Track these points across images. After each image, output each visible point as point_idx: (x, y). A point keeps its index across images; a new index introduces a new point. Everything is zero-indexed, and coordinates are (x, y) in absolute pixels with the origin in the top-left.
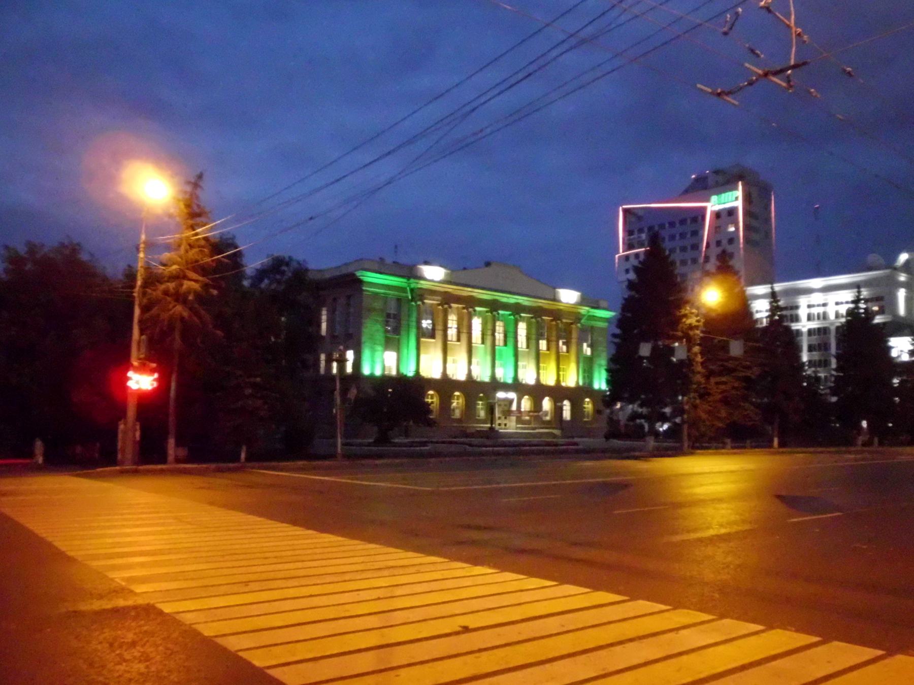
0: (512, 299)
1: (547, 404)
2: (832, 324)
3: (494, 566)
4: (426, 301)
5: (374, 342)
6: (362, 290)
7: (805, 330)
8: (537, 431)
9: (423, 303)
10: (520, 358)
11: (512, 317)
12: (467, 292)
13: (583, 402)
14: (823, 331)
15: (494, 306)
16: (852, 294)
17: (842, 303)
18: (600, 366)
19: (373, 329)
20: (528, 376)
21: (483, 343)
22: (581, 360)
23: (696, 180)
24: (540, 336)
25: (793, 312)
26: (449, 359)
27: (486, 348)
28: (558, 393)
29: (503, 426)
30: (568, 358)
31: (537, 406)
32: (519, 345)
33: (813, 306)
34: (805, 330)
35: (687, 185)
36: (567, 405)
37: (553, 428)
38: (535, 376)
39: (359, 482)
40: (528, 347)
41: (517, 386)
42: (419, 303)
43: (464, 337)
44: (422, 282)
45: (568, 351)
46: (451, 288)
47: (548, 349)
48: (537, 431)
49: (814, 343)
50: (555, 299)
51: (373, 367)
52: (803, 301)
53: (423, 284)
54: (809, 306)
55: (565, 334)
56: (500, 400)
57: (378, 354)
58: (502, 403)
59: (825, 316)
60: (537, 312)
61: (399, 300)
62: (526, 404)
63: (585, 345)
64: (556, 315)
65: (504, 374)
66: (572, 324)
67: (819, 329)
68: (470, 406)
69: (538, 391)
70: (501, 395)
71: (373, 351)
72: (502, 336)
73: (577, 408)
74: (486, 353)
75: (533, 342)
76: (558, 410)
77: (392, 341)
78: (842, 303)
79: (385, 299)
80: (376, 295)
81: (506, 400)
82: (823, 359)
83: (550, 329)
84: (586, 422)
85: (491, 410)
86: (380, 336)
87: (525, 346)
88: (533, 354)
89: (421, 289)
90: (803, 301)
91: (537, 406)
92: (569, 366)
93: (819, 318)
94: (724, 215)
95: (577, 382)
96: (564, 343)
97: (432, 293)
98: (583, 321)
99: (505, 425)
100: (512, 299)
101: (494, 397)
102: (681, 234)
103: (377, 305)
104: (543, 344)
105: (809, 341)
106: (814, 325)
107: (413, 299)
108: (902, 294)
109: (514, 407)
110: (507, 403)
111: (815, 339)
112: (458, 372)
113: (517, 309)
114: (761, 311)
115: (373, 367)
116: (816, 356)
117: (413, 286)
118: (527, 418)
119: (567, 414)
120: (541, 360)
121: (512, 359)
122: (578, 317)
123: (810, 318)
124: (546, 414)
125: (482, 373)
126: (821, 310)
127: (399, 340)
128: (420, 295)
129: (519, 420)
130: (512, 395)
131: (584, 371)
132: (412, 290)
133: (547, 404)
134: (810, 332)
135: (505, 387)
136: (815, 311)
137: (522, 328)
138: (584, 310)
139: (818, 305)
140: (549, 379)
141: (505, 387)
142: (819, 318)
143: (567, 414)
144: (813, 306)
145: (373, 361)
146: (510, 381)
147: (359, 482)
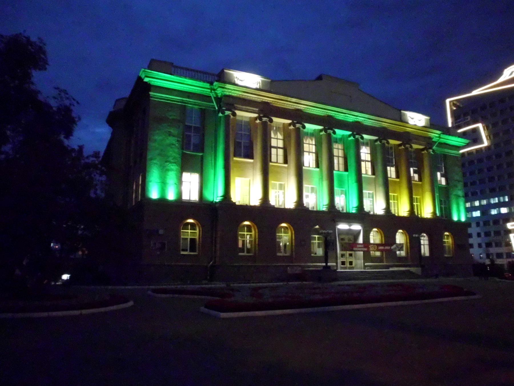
0: (351, 117)
1: (400, 238)
3: (363, 125)
4: (238, 113)
5: (165, 159)
6: (150, 100)
8: (391, 269)
9: (234, 114)
10: (364, 185)
12: (291, 103)
13: (442, 236)
15: (329, 123)
18: (458, 196)
19: (164, 140)
20: (376, 205)
21: (318, 166)
22: (436, 190)
24: (387, 163)
26: (272, 182)
27: (321, 171)
28: (413, 224)
29: (348, 265)
30: (422, 186)
31: (389, 239)
32: (363, 171)
36: (424, 241)
37: (410, 266)
38: (384, 205)
39: (45, 314)
40: (373, 173)
41: (362, 216)
42: (227, 113)
43: (292, 158)
44: (228, 86)
45: (420, 179)
46: (269, 98)
47: (398, 176)
48: (391, 269)
50: (401, 119)
51: (163, 190)
53: (230, 90)
55: (416, 160)
56: (341, 232)
57: (172, 177)
58: (346, 237)
60: (383, 134)
61: (203, 113)
62: (375, 237)
63: (439, 174)
64: (407, 137)
65: (346, 202)
66: (423, 150)
68: (302, 242)
69: (389, 223)
70: (342, 226)
71: (164, 171)
72: (341, 160)
73: (435, 244)
74: (321, 179)
75: (379, 168)
76: (414, 244)
77: (192, 159)
79: (183, 109)
80: (169, 106)
81: (349, 232)
83: (398, 155)
84: (447, 258)
85: (329, 245)
86: (174, 153)
87: (370, 172)
88: (380, 180)
89: (229, 96)
91: (389, 239)
92: (423, 197)
95: (434, 213)
96: (415, 172)
97: (246, 103)
98: (434, 147)
99: (351, 263)
100: (351, 117)
101: (334, 229)
103: (172, 115)
104: (392, 171)
107: (220, 110)
109: (361, 240)
110: (351, 237)
112: (284, 196)
113: (357, 128)
115: (163, 190)
117: (220, 92)
118: (378, 254)
119: (425, 250)
122: (429, 142)
124: (400, 247)
125: (316, 200)
127: (202, 158)
128: (231, 103)
129: (367, 257)
130: (357, 227)
131: (441, 202)
132: (219, 100)
133: (400, 238)
135: (348, 217)
137: (365, 153)
138: (435, 134)
140: (402, 209)
141: (348, 217)
143: (425, 250)
145: (164, 183)
147: (45, 314)
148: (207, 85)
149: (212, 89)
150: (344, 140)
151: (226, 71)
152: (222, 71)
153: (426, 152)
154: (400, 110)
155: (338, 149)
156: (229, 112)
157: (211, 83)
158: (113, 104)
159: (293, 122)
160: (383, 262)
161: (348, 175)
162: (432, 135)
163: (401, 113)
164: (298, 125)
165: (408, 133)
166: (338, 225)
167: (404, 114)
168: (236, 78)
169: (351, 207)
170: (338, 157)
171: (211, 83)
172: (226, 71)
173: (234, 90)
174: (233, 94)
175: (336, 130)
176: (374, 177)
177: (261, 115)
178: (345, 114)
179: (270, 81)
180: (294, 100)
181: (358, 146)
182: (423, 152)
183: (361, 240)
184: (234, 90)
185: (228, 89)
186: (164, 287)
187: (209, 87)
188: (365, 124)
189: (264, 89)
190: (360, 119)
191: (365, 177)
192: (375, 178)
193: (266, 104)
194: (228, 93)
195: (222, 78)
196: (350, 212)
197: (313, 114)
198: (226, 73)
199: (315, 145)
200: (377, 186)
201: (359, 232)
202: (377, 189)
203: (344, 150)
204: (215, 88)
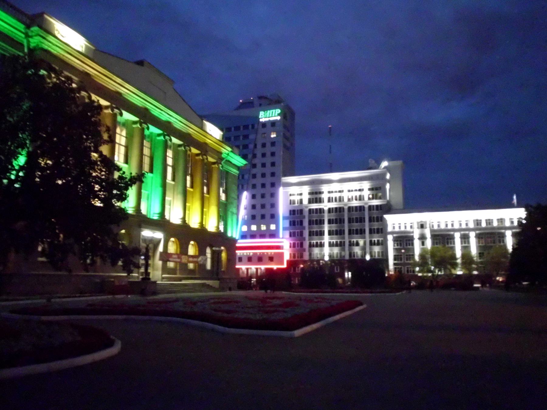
1: (192, 250)
2: (346, 205)
3: (191, 137)
7: (326, 209)
8: (184, 282)
11: (162, 138)
14: (339, 210)
16: (369, 184)
17: (352, 191)
20: (174, 216)
23: (242, 103)
25: (318, 196)
28: (203, 237)
31: (184, 250)
33: (332, 192)
34: (326, 209)
35: (239, 104)
41: (162, 224)
44: (50, 38)
48: (184, 282)
49: (331, 218)
50: (202, 127)
52: (325, 188)
54: (329, 192)
59: (341, 199)
64: (204, 148)
66: (214, 163)
67: (336, 208)
69: (183, 233)
70: (147, 233)
75: (180, 174)
78: (352, 191)
82: (338, 229)
88: (180, 188)
90: (325, 188)
91: (184, 250)
93: (336, 201)
94: (269, 126)
102: (235, 137)
105: (329, 216)
106: (333, 205)
108: (388, 186)
109: (161, 248)
111: (333, 216)
113: (168, 129)
114: (293, 195)
116: (334, 227)
117: (35, 41)
120: (189, 198)
121: (159, 190)
123: (330, 200)
126: (338, 195)
130: (159, 235)
133: (192, 250)
134: (330, 210)
136: (333, 195)
139: (336, 192)
142: (336, 201)
144: (332, 192)
146: (156, 217)
148: (21, 27)
149: (27, 36)
150: (152, 137)
151: (46, 17)
152: (41, 15)
153: (216, 166)
154: (202, 120)
155: (121, 135)
156: (85, 93)
157: (28, 27)
158: (474, 292)
159: (140, 120)
160: (175, 274)
161: (152, 177)
162: (223, 151)
163: (202, 122)
164: (116, 111)
165: (206, 144)
166: (142, 231)
167: (205, 124)
168: (57, 30)
169: (152, 213)
170: (120, 144)
171: (28, 27)
172: (46, 17)
173: (57, 46)
174: (52, 51)
175: (172, 138)
176: (173, 183)
177: (114, 106)
178: (162, 110)
179: (94, 48)
180: (119, 80)
181: (166, 147)
182: (213, 166)
183: (161, 248)
184: (57, 46)
185: (50, 42)
186: (101, 274)
187: (23, 31)
188: (175, 126)
189: (87, 54)
190: (172, 120)
191: (169, 183)
192: (174, 185)
193: (189, 135)
194: (46, 47)
195: (34, 20)
196: (151, 217)
197: (109, 89)
198: (46, 19)
199: (126, 137)
200: (175, 193)
201: (159, 241)
202: (175, 196)
203: (151, 149)
204: (30, 34)
